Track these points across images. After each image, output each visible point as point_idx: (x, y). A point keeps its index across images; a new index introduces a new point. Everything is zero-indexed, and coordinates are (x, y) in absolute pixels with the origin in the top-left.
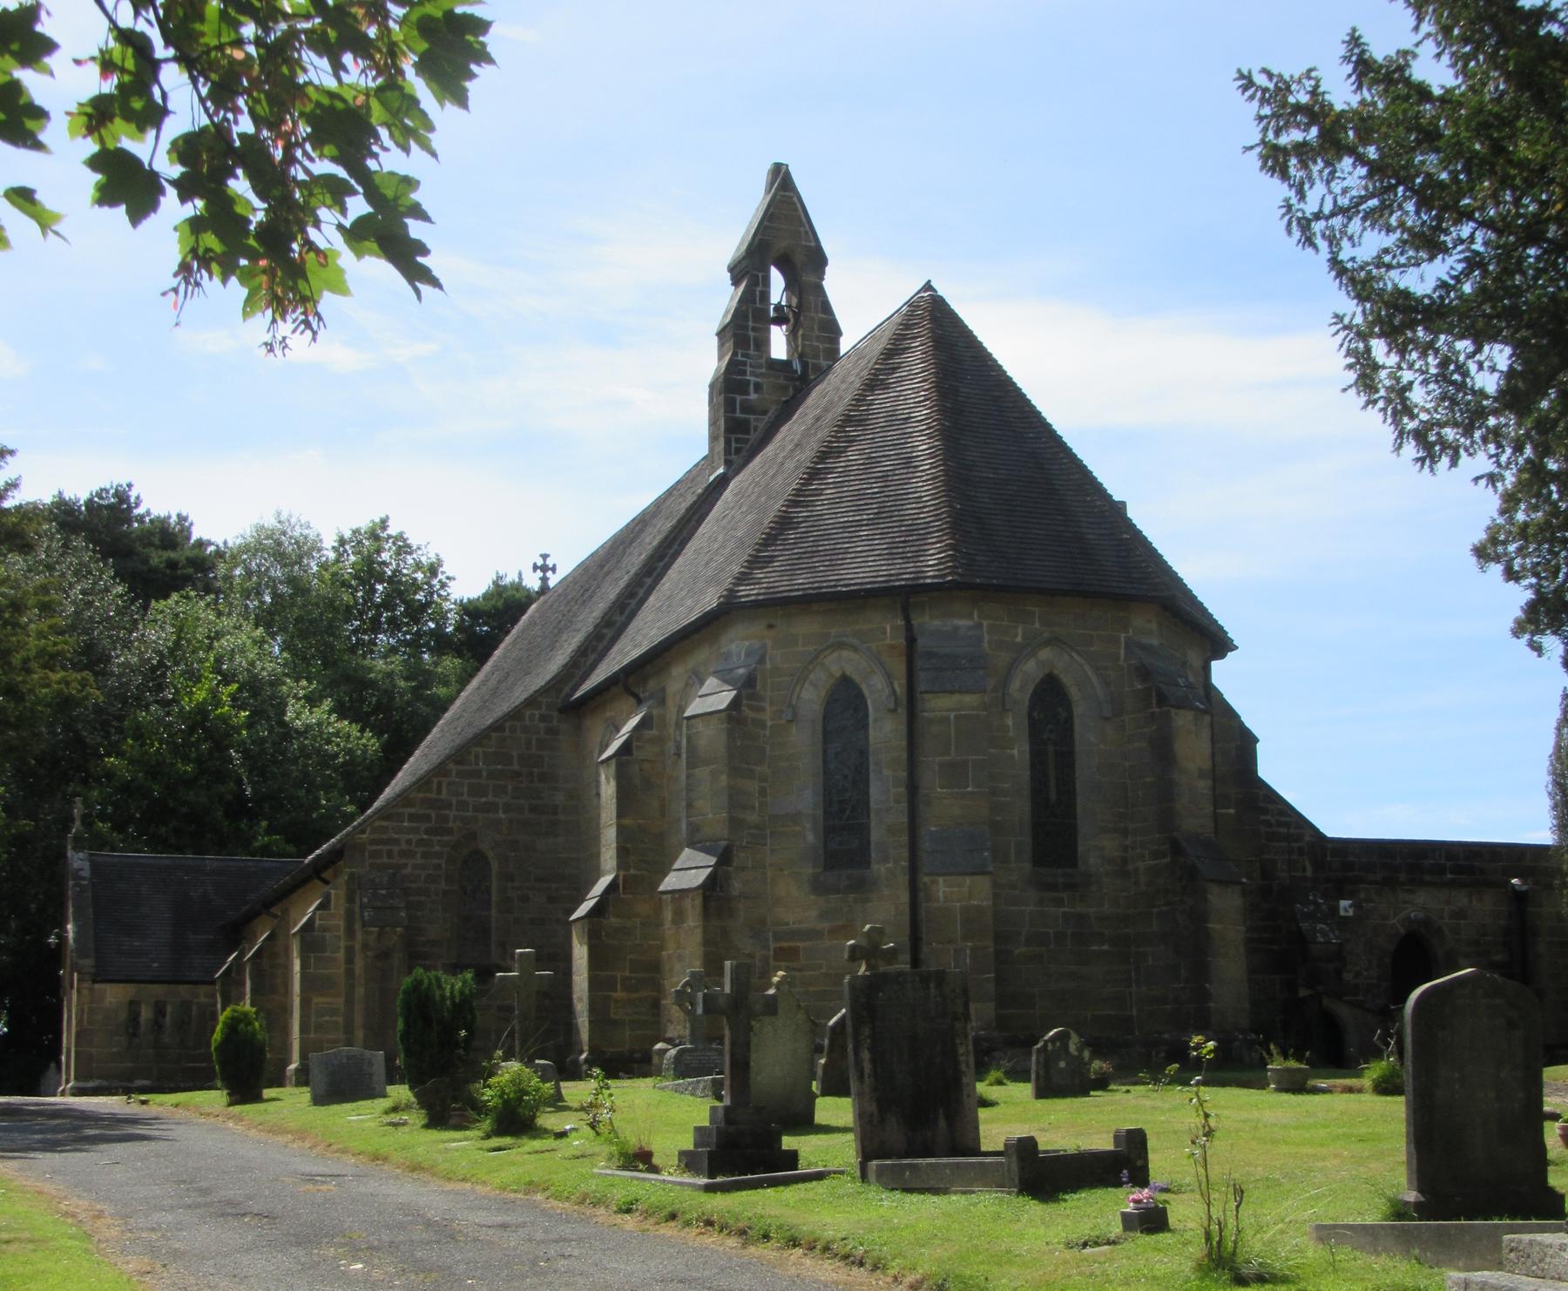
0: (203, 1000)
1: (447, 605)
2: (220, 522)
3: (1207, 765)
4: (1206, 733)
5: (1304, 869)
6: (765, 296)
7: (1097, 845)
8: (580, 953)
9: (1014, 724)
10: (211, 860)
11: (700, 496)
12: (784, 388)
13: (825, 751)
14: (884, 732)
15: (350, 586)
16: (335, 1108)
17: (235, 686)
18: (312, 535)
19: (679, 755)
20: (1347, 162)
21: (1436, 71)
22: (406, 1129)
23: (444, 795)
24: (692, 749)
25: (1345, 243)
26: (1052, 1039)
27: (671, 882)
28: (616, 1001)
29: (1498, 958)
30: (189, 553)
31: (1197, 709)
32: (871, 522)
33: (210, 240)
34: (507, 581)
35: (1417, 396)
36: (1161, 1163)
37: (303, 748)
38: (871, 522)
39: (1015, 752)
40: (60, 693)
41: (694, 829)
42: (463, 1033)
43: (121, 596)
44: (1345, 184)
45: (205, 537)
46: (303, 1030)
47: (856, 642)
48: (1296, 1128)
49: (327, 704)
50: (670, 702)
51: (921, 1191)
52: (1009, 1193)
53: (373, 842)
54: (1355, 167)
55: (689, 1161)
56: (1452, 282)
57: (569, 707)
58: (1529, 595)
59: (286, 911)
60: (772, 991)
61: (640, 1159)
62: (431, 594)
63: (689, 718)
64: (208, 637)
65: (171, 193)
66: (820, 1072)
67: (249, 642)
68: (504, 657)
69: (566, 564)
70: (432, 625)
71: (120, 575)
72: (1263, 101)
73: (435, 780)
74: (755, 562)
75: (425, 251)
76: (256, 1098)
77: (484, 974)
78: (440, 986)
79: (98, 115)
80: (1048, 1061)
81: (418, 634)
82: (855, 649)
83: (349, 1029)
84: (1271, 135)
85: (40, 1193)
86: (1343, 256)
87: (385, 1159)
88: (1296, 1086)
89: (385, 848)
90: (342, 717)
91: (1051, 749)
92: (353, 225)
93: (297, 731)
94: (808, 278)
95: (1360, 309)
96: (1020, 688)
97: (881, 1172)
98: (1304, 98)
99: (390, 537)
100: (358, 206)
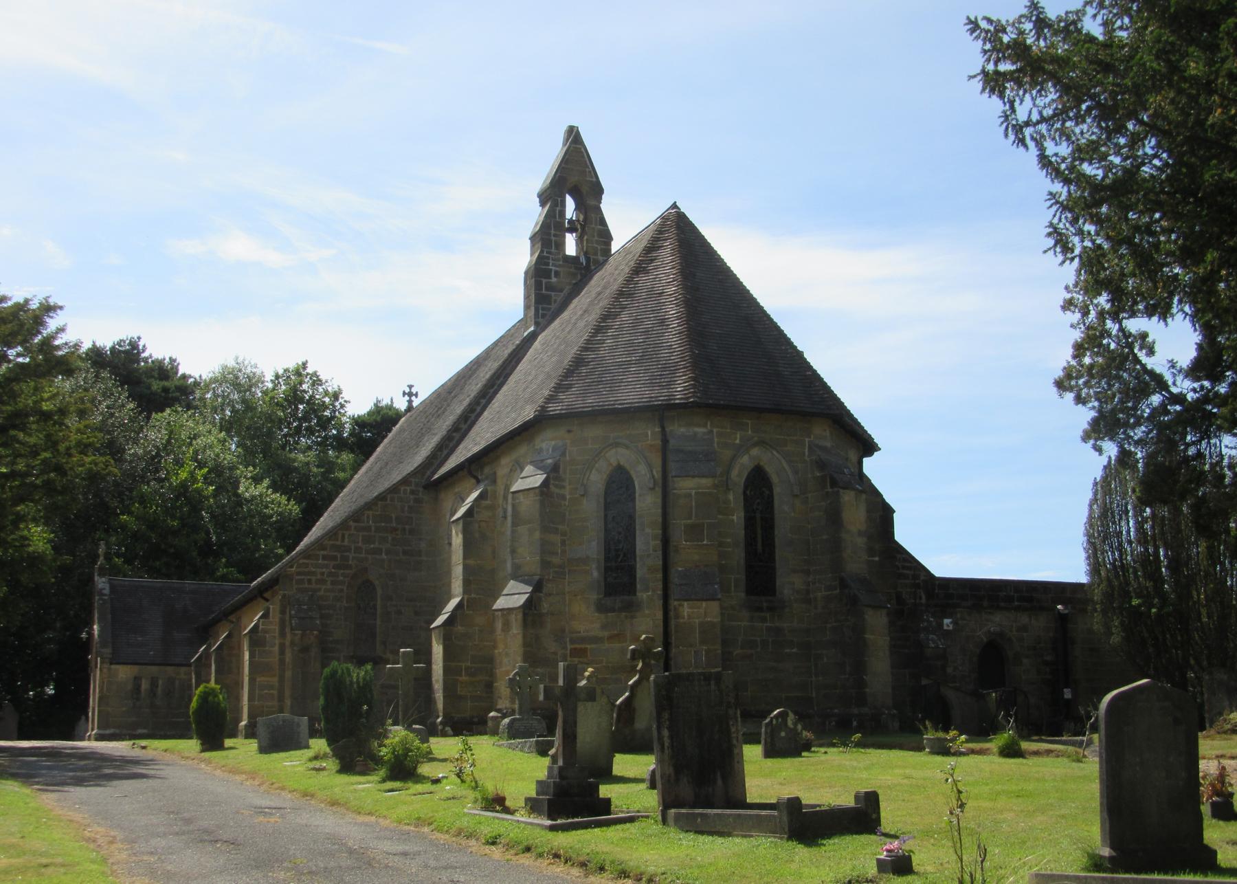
1: (344, 419)
2: (198, 361)
6: (563, 213)
7: (789, 582)
8: (438, 650)
9: (734, 498)
10: (189, 584)
11: (518, 346)
13: (606, 516)
14: (647, 504)
16: (275, 756)
18: (258, 372)
19: (505, 517)
22: (325, 773)
23: (346, 543)
26: (776, 717)
27: (501, 603)
29: (1049, 658)
30: (177, 383)
32: (638, 362)
34: (383, 404)
36: (889, 816)
37: (249, 510)
38: (638, 362)
40: (90, 470)
41: (517, 567)
46: (250, 700)
49: (266, 482)
50: (499, 481)
51: (711, 833)
52: (781, 838)
53: (299, 574)
55: (533, 806)
57: (430, 484)
58: (1093, 414)
59: (239, 619)
61: (497, 803)
62: (334, 412)
68: (383, 452)
69: (424, 392)
70: (334, 432)
71: (132, 396)
72: (985, 40)
73: (340, 533)
78: (349, 675)
80: (773, 730)
81: (326, 438)
82: (627, 447)
83: (281, 698)
85: (71, 821)
87: (312, 796)
90: (275, 491)
91: (758, 515)
95: (1066, 189)
96: (738, 475)
97: (678, 818)
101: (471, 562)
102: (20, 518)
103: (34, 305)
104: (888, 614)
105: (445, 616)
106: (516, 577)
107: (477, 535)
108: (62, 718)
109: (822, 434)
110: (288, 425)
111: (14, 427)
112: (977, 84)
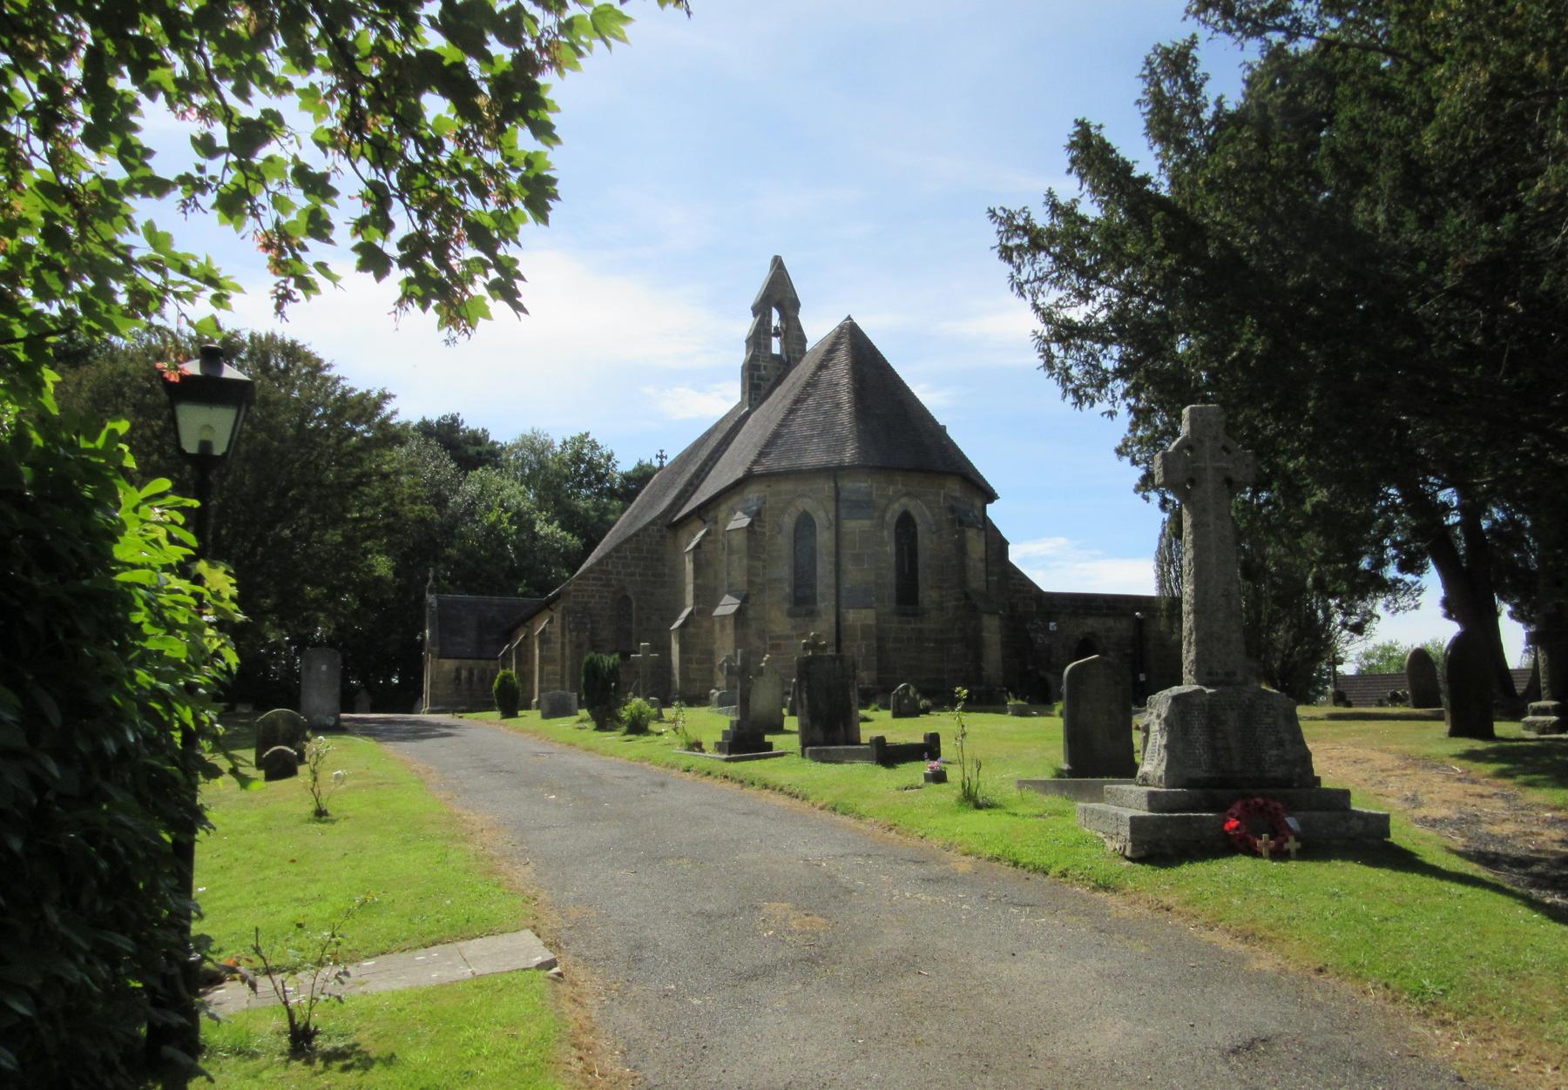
2: (503, 433)
6: (770, 322)
7: (928, 595)
9: (888, 535)
10: (496, 599)
14: (824, 538)
21: (1091, 209)
33: (417, 289)
35: (1074, 372)
36: (947, 749)
38: (820, 435)
41: (730, 585)
49: (556, 523)
55: (720, 747)
57: (672, 525)
58: (1143, 472)
61: (697, 746)
65: (395, 264)
69: (672, 455)
71: (453, 458)
74: (762, 454)
77: (625, 656)
79: (361, 225)
80: (899, 700)
83: (562, 682)
86: (1039, 302)
88: (1021, 712)
94: (790, 313)
96: (891, 517)
98: (1021, 222)
100: (493, 274)
102: (367, 552)
103: (374, 395)
106: (730, 593)
108: (407, 699)
109: (954, 488)
110: (574, 482)
111: (363, 484)
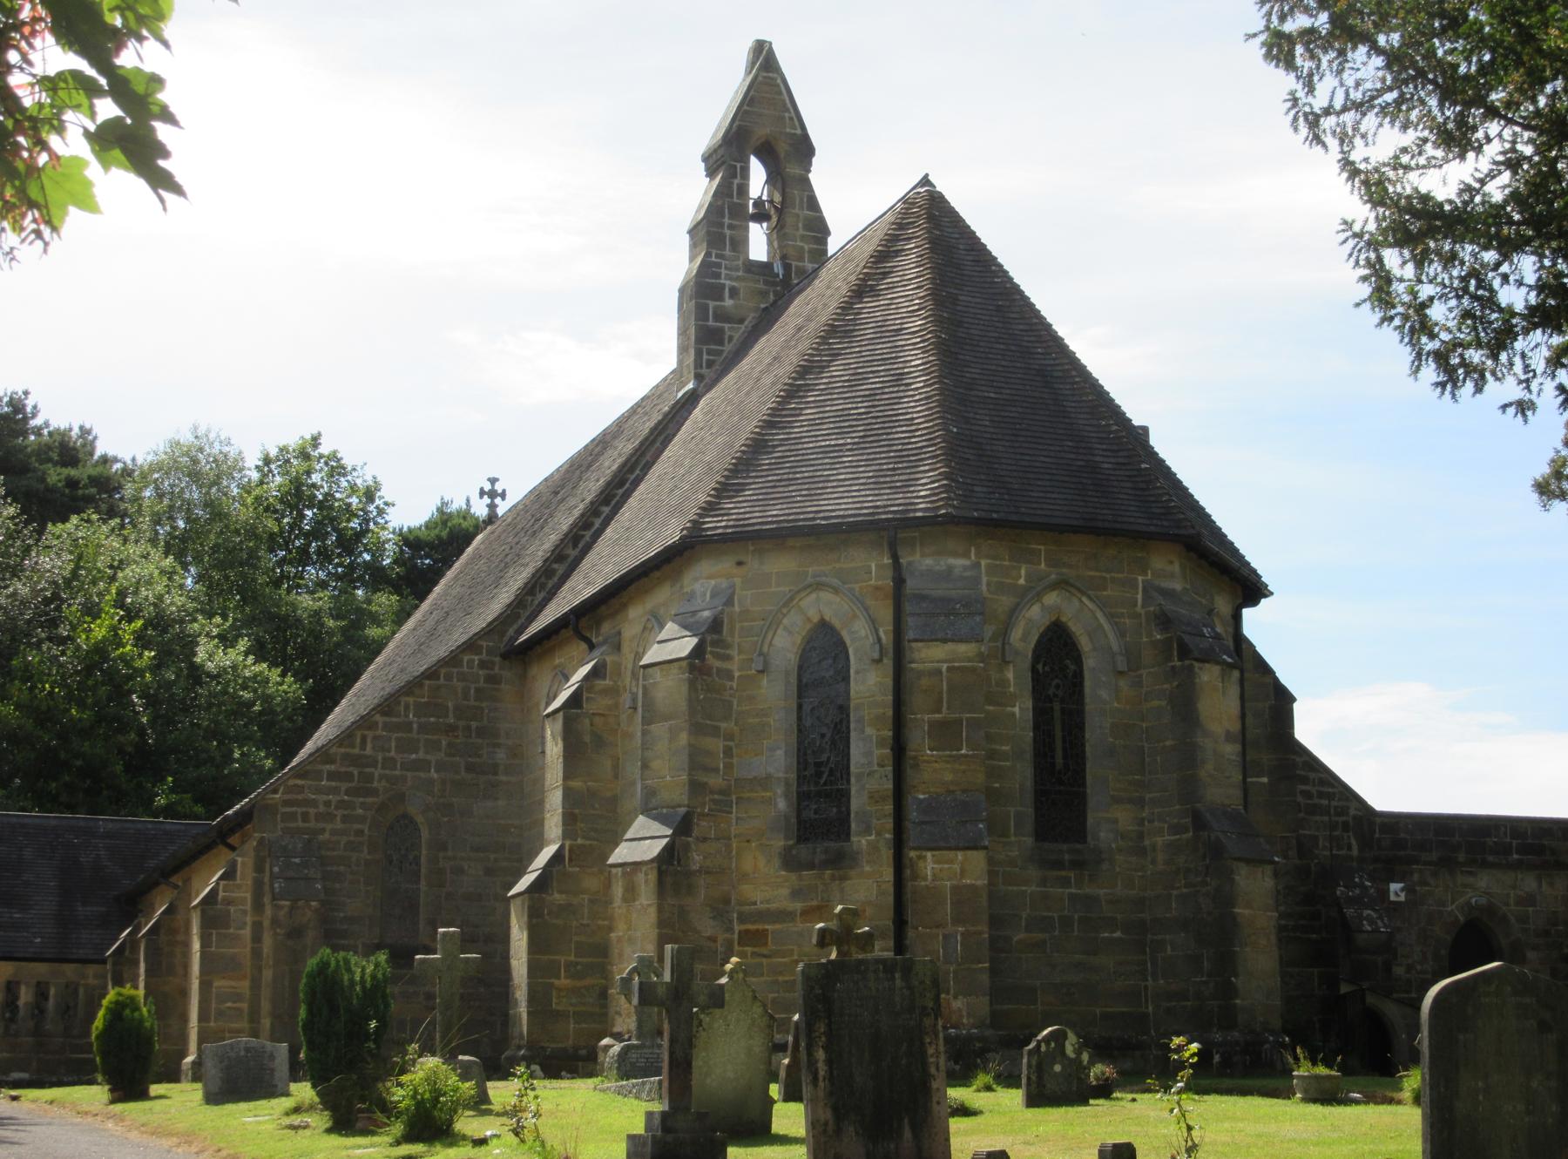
0: (91, 981)
2: (128, 438)
3: (1235, 727)
4: (1234, 691)
5: (1350, 847)
6: (743, 190)
7: (1109, 818)
8: (519, 939)
9: (1016, 678)
10: (105, 822)
11: (666, 415)
12: (764, 294)
13: (800, 707)
14: (868, 685)
15: (276, 511)
16: (230, 1107)
17: (140, 623)
20: (1362, 50)
22: (308, 1132)
23: (369, 751)
24: (649, 704)
25: (1358, 141)
26: (1047, 1039)
28: (559, 990)
30: (94, 472)
31: (1225, 662)
34: (454, 507)
35: (1437, 312)
39: (1017, 710)
41: (650, 793)
42: (373, 1024)
43: (12, 518)
44: (1359, 75)
45: (111, 453)
46: (203, 1017)
47: (835, 582)
48: (1317, 1144)
49: (243, 644)
50: (625, 648)
53: (286, 803)
54: (1369, 56)
56: (1477, 185)
57: (515, 650)
59: (188, 880)
60: (724, 980)
62: (367, 521)
63: (645, 667)
64: (111, 567)
66: (782, 1074)
67: (156, 572)
68: (445, 594)
69: (517, 490)
70: (367, 557)
73: (359, 734)
75: (165, 154)
76: (143, 1095)
77: (402, 956)
78: (349, 970)
80: (1040, 1067)
81: (352, 567)
82: (836, 591)
83: (254, 1016)
84: (1274, 18)
86: (1355, 156)
88: (1326, 1095)
89: (299, 810)
91: (1057, 707)
92: (99, 128)
93: (209, 675)
94: (793, 170)
95: (1373, 215)
99: (321, 456)
101: (576, 784)
104: (1276, 875)
105: (535, 875)
106: (647, 811)
107: (587, 739)
109: (1168, 570)
110: (289, 544)
112: (1256, 49)
